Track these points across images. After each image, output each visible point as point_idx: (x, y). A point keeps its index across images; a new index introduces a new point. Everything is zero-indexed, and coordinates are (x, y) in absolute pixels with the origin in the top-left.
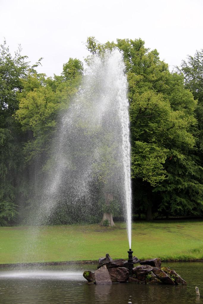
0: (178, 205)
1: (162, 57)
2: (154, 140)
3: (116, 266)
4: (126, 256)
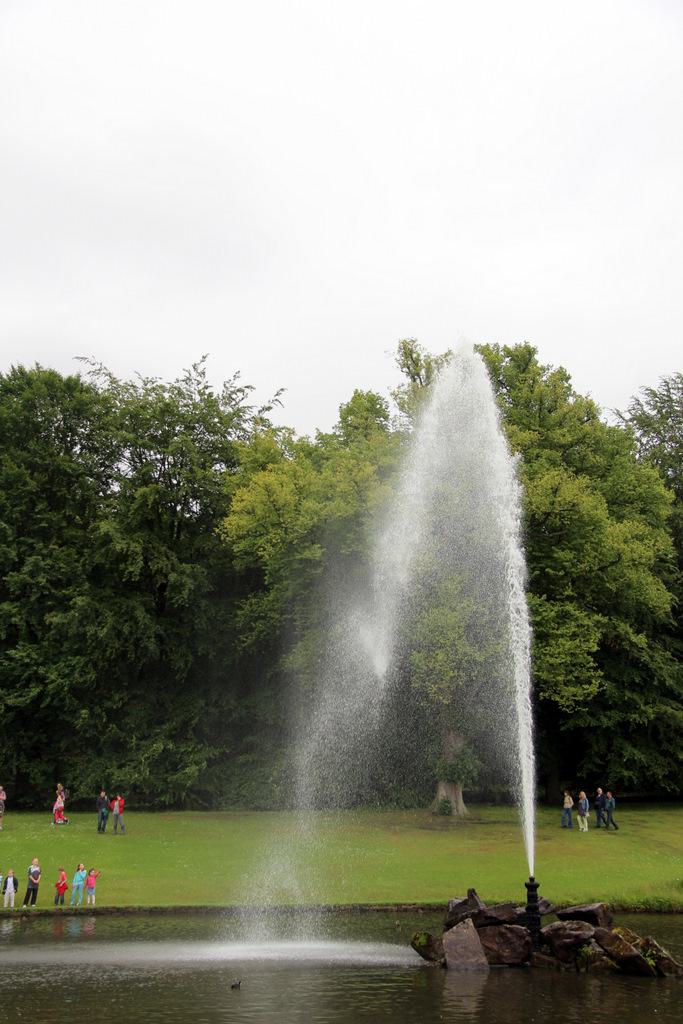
2: (569, 592)
4: (522, 896)
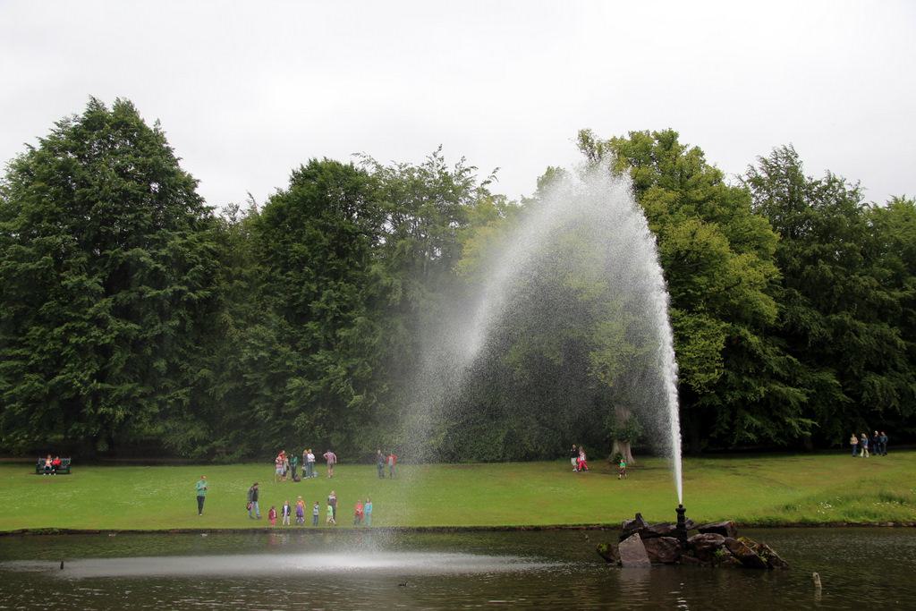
0: (748, 430)
1: (711, 159)
3: (656, 535)
4: (673, 518)
